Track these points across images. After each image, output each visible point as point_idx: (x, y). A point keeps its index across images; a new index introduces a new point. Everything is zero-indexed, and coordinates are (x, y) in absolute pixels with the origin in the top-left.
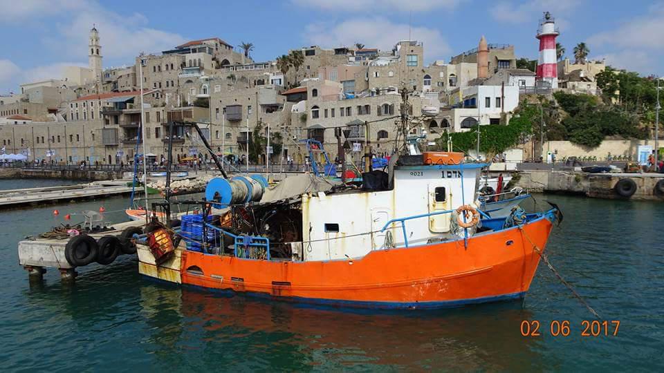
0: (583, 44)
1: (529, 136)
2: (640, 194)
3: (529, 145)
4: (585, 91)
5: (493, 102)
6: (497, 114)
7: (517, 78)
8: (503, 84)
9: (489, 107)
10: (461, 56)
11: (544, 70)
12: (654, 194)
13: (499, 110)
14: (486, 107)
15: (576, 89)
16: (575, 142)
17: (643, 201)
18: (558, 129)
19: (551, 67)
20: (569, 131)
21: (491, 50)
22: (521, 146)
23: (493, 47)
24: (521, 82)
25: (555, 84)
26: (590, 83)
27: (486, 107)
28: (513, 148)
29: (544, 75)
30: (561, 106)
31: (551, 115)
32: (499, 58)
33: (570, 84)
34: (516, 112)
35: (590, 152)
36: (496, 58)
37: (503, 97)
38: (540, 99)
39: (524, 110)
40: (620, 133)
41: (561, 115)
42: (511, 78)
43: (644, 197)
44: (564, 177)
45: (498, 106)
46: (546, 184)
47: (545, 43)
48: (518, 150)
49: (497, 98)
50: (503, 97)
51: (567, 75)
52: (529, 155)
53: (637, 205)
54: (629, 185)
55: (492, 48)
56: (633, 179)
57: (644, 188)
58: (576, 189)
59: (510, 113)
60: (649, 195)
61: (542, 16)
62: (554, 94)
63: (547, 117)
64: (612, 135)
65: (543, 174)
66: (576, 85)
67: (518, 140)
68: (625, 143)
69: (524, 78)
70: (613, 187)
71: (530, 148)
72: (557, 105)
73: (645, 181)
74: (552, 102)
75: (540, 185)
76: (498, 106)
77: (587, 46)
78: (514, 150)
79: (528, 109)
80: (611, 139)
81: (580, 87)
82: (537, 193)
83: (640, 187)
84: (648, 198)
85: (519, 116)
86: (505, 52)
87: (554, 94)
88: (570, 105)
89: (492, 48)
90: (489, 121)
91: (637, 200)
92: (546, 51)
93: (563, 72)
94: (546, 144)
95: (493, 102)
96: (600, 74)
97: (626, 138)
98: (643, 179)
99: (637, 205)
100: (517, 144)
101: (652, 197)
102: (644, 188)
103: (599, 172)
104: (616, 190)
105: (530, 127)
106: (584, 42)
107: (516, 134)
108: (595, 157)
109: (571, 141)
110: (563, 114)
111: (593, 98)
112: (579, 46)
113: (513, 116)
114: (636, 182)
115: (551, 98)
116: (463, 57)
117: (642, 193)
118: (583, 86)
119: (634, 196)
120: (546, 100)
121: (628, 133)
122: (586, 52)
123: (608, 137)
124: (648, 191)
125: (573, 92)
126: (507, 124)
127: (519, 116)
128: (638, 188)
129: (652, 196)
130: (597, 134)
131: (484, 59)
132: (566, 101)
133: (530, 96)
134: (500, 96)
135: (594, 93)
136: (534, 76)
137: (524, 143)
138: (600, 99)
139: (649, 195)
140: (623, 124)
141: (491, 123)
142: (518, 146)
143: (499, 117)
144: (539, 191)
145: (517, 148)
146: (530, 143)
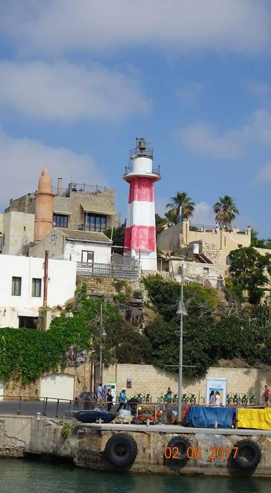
0: (227, 198)
1: (84, 352)
2: (144, 463)
3: (86, 369)
4: (198, 278)
5: (27, 286)
6: (33, 309)
7: (79, 247)
8: (47, 254)
9: (20, 294)
10: (23, 199)
11: (134, 235)
12: (164, 464)
13: (38, 302)
14: (14, 294)
15: (184, 273)
16: (162, 368)
17: (149, 474)
18: (136, 342)
19: (146, 232)
20: (156, 346)
21: (72, 194)
22: (70, 370)
23: (78, 188)
24: (85, 254)
25: (148, 263)
26: (206, 265)
27: (14, 294)
28: (55, 373)
29: (134, 245)
30: (153, 302)
31: (128, 316)
32: (88, 209)
33: (174, 265)
34: (69, 307)
35: (191, 387)
36: (82, 208)
37: (46, 277)
38: (118, 286)
39: (80, 305)
40: (244, 356)
41: (146, 318)
42: (68, 246)
43: (150, 468)
44: (50, 429)
45: (36, 293)
46: (28, 442)
47: (137, 191)
48: (65, 378)
49: (35, 280)
50: (46, 277)
51: (185, 249)
52: (85, 387)
53: (138, 479)
54: (123, 445)
55: (74, 190)
56: (135, 434)
57: (150, 451)
58: (64, 451)
59: (59, 308)
60: (158, 464)
61: (134, 144)
62: (144, 281)
63: (120, 320)
64: (231, 359)
65: (24, 422)
66: (185, 267)
67: (65, 359)
68: (247, 373)
69: (90, 248)
70: (103, 449)
71: (88, 376)
72: (146, 298)
73: (152, 437)
74: (138, 295)
75: (19, 444)
76: (36, 293)
77: (236, 203)
78: (58, 378)
79: (87, 304)
80: (228, 365)
81: (191, 272)
82: (13, 458)
83: (144, 450)
84: (156, 469)
85: (71, 315)
86: (99, 200)
87: (144, 281)
88: (165, 301)
89: (74, 190)
90: (18, 320)
91: (139, 474)
92: (137, 204)
93: (178, 244)
94: (112, 368)
95: (27, 286)
96: (237, 251)
97: (252, 364)
98: (149, 435)
99: (138, 479)
100: (63, 367)
101: (162, 468)
102: (150, 451)
103: (94, 421)
104: (105, 455)
105: (88, 337)
106: (229, 195)
107: (61, 349)
108: (193, 396)
109: (155, 365)
110: (150, 315)
111: (209, 291)
112: (222, 201)
113: (63, 315)
114: (138, 441)
115: (137, 286)
116: (27, 203)
117: (147, 461)
118: (195, 270)
119: (135, 467)
120: (129, 290)
121: (258, 357)
122: (232, 212)
123: (222, 361)
124: (156, 456)
125: (179, 279)
126: (48, 327)
127: (71, 315)
128: (140, 452)
129: (162, 467)
130: (198, 356)
131: (46, 209)
132: (164, 294)
133: (99, 280)
134: (41, 276)
135: (214, 284)
136: (109, 245)
137: (76, 366)
138: (221, 295)
139: (158, 464)
140: (249, 338)
141: (21, 325)
142: (66, 371)
143: (36, 314)
144: (16, 455)
145: (63, 374)
146: (88, 366)
